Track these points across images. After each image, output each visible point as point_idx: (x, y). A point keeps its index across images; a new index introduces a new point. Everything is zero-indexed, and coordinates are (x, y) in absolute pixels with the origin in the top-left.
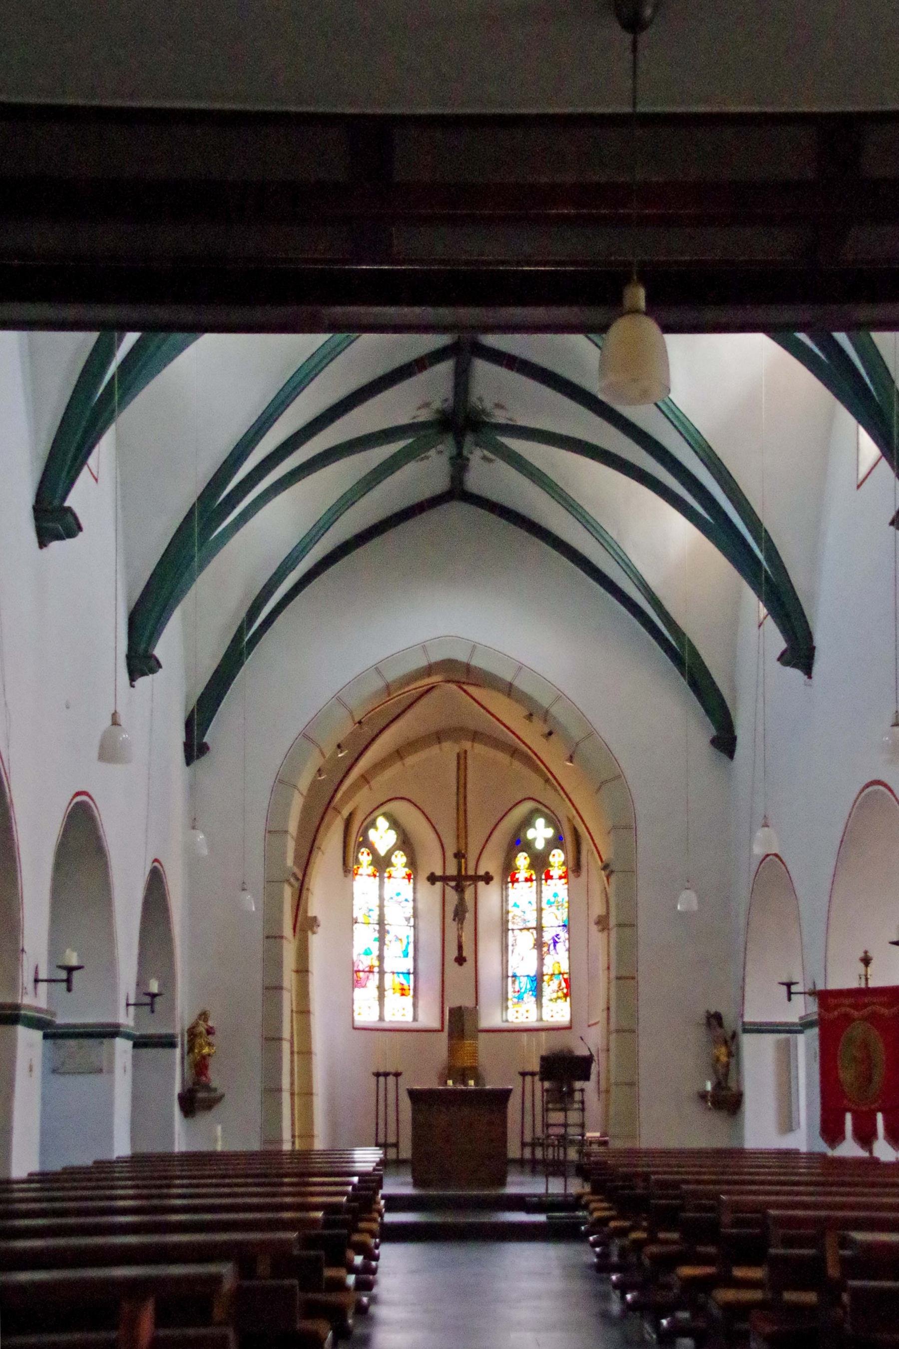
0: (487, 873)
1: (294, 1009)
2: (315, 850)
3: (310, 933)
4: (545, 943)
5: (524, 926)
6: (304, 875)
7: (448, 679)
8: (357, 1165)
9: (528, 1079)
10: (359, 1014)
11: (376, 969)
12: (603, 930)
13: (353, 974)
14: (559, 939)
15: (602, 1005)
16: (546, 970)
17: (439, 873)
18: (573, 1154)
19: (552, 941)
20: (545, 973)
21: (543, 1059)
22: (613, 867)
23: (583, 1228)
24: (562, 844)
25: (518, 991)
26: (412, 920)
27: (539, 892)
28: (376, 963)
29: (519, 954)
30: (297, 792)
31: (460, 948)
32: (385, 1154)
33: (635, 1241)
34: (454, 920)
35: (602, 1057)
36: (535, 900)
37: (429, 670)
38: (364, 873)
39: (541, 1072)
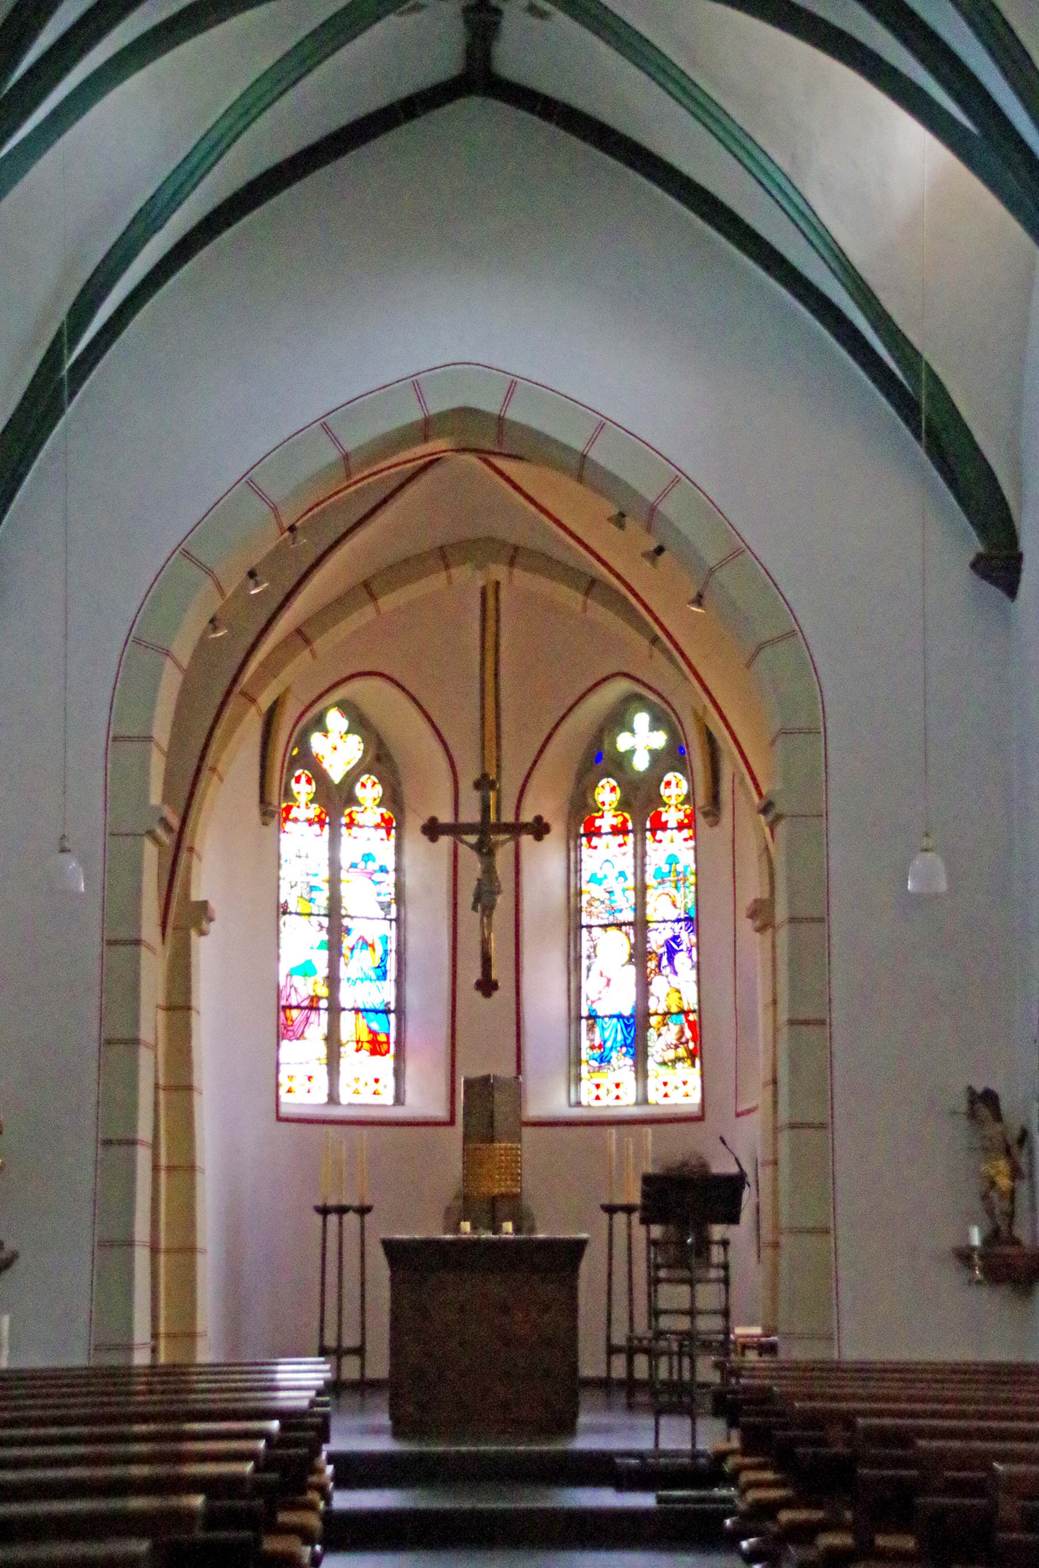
0: (539, 819)
1: (162, 1082)
2: (205, 773)
3: (193, 934)
4: (650, 953)
5: (611, 920)
6: (184, 821)
7: (463, 445)
8: (282, 1394)
9: (620, 1218)
10: (289, 1091)
11: (324, 1004)
12: (761, 929)
13: (278, 1013)
14: (678, 945)
15: (764, 1073)
16: (653, 1005)
17: (445, 817)
18: (707, 1371)
19: (664, 949)
20: (652, 1011)
21: (647, 1180)
22: (779, 808)
23: (728, 1522)
24: (685, 768)
25: (600, 1046)
26: (394, 907)
27: (640, 857)
28: (323, 991)
29: (601, 974)
30: (169, 663)
31: (486, 962)
32: (338, 1369)
33: (832, 1552)
34: (474, 908)
35: (765, 1175)
36: (632, 870)
37: (426, 429)
38: (302, 818)
39: (644, 1208)
